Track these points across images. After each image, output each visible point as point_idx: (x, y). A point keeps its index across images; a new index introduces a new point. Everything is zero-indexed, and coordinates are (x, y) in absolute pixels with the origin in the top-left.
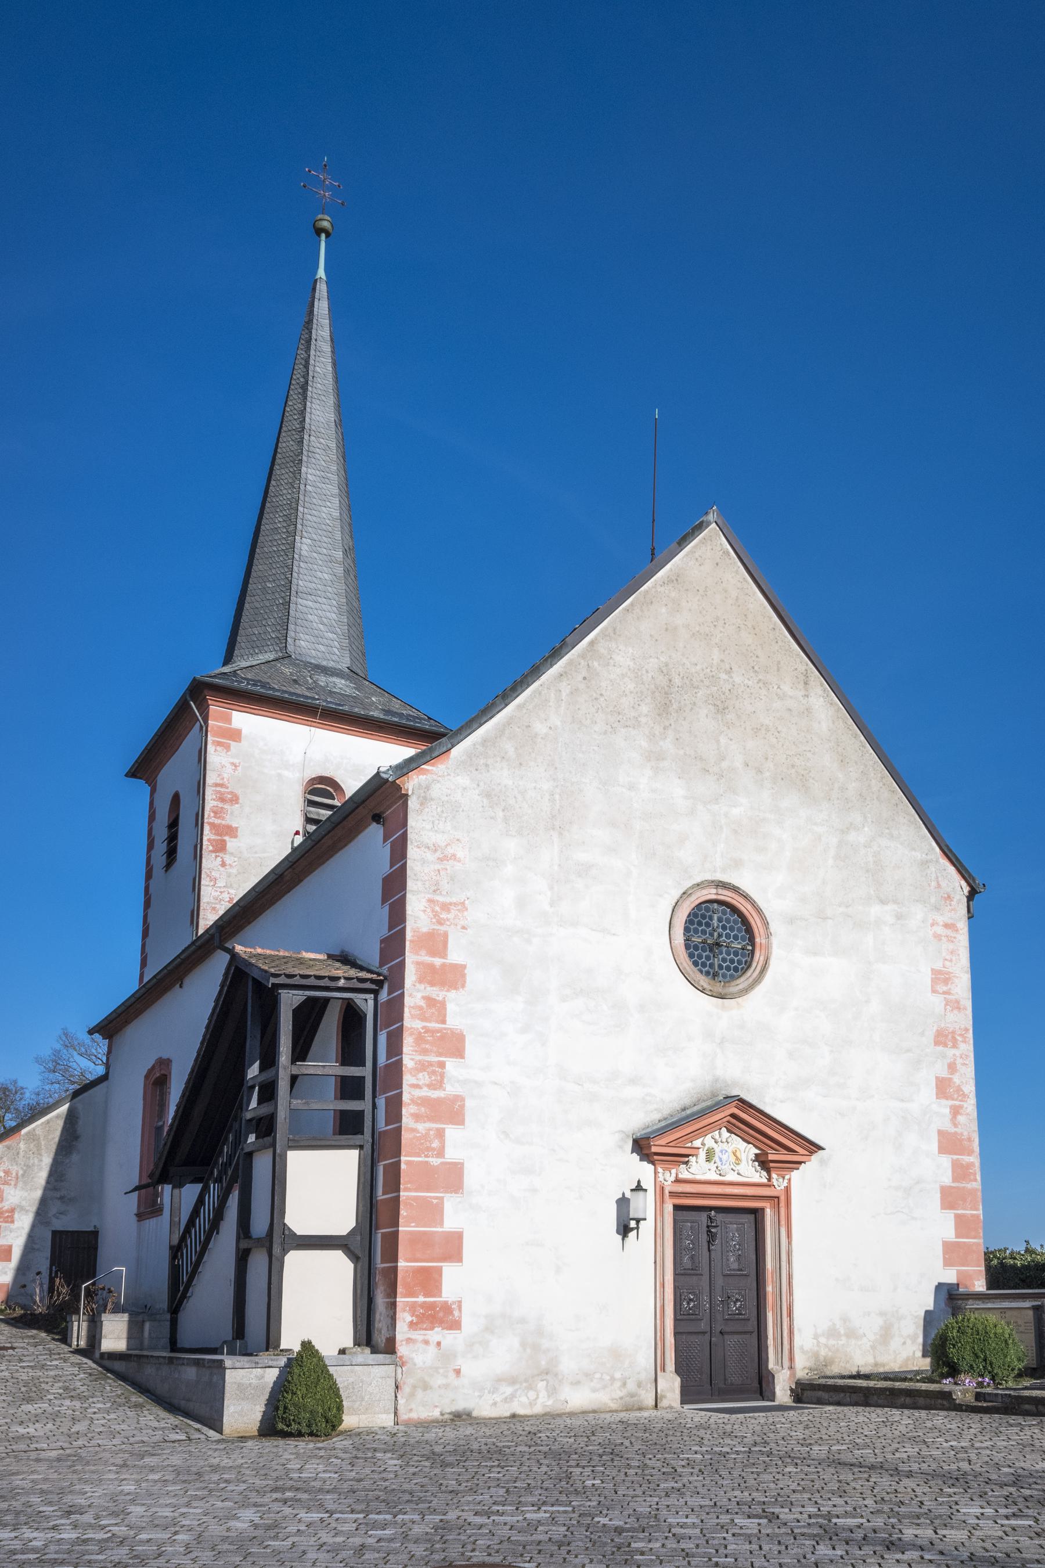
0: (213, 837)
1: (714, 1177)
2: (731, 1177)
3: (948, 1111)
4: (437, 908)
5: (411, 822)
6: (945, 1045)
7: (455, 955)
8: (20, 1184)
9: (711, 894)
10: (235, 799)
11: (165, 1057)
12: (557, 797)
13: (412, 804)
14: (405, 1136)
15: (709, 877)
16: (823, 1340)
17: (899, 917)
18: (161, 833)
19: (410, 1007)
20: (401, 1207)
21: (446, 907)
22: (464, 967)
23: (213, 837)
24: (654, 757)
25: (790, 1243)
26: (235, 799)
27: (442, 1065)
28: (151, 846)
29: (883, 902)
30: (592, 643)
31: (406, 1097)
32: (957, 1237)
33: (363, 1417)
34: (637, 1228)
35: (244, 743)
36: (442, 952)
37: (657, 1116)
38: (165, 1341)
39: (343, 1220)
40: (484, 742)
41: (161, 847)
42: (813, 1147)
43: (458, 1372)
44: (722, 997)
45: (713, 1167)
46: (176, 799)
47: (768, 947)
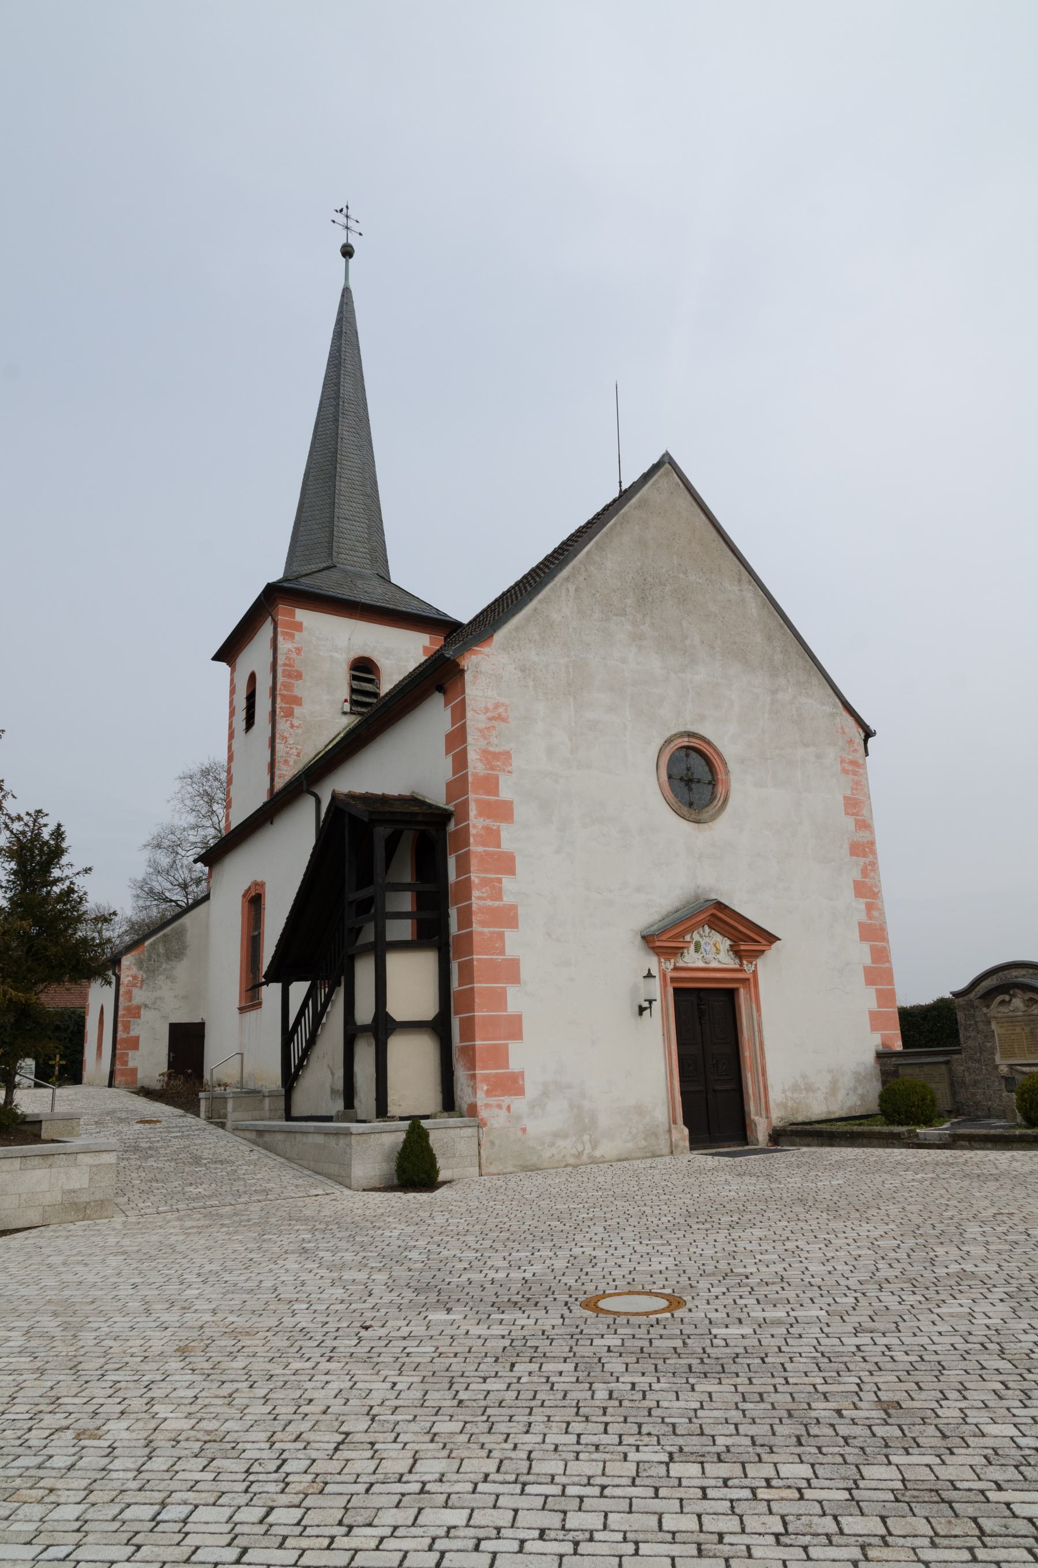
0: (284, 705)
1: (700, 964)
2: (714, 965)
3: (864, 906)
4: (490, 757)
5: (467, 691)
6: (858, 856)
7: (505, 793)
8: (145, 987)
9: (685, 742)
10: (299, 676)
11: (259, 880)
12: (571, 670)
13: (468, 676)
14: (476, 938)
15: (682, 729)
16: (789, 1094)
17: (818, 756)
18: (241, 703)
19: (474, 835)
20: (476, 995)
21: (496, 756)
22: (512, 802)
23: (284, 705)
24: (637, 638)
25: (760, 1016)
26: (299, 676)
27: (500, 881)
28: (232, 713)
29: (806, 745)
30: (588, 553)
31: (474, 907)
32: (879, 1006)
33: (456, 1170)
34: (650, 1007)
35: (305, 633)
36: (496, 793)
37: (657, 917)
38: (282, 1112)
39: (426, 1008)
40: (517, 629)
41: (241, 715)
42: (772, 939)
43: (524, 1130)
44: (698, 822)
45: (699, 956)
46: (253, 677)
47: (727, 783)
